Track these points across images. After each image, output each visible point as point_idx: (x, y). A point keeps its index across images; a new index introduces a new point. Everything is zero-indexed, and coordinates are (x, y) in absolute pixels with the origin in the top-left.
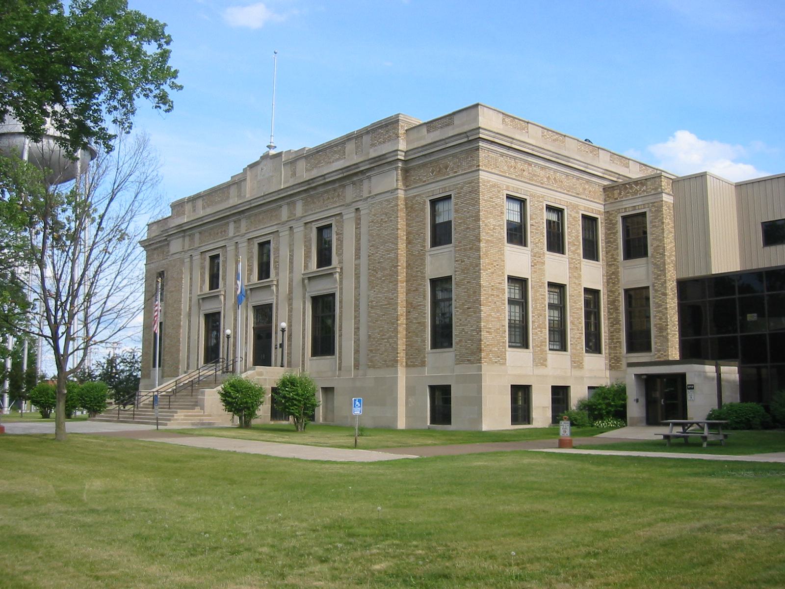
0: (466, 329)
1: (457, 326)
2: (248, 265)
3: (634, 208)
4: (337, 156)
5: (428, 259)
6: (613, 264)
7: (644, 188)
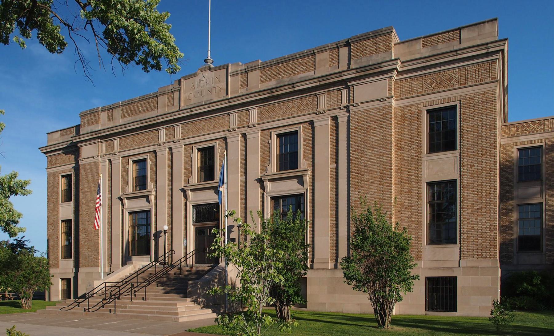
0: (476, 227)
1: (464, 225)
2: (185, 169)
3: (531, 142)
4: (304, 68)
5: (424, 165)
6: (508, 185)
7: (542, 127)
